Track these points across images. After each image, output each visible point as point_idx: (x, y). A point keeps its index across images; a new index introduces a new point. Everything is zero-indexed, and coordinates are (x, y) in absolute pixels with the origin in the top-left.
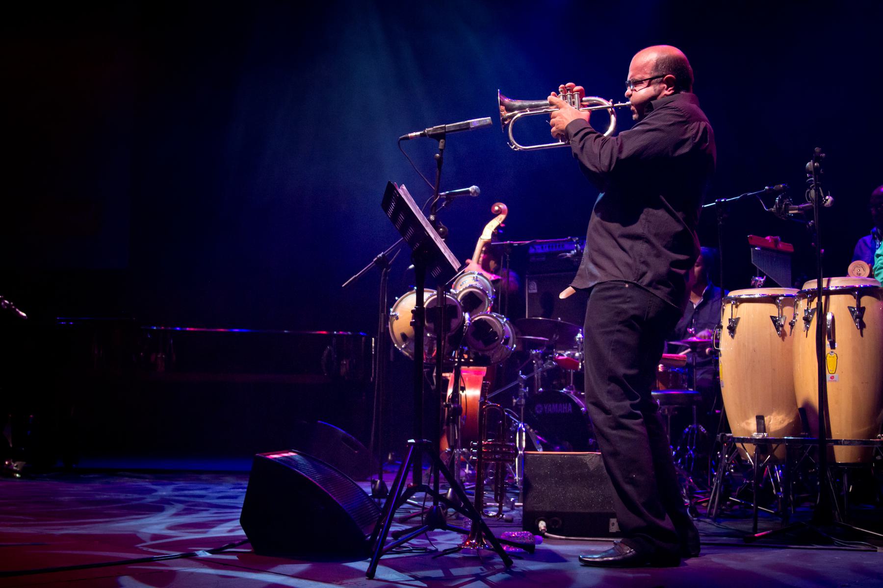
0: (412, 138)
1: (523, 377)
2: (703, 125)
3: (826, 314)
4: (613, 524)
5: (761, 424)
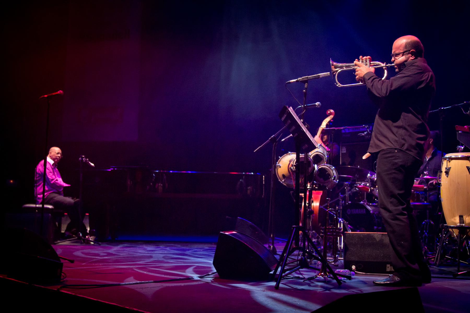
0: (292, 82)
2: (431, 73)
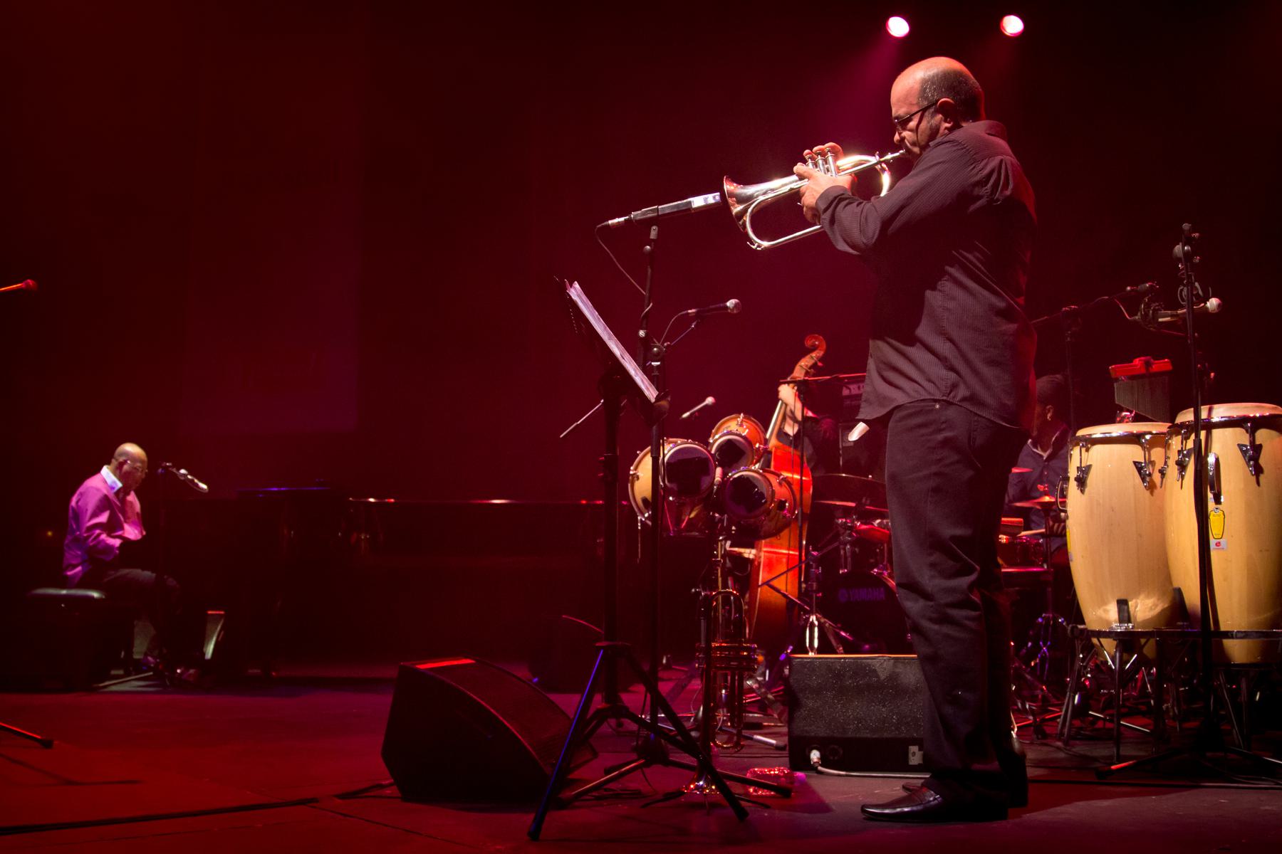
1: (815, 553)
3: (1207, 455)
4: (914, 754)
5: (1125, 615)
